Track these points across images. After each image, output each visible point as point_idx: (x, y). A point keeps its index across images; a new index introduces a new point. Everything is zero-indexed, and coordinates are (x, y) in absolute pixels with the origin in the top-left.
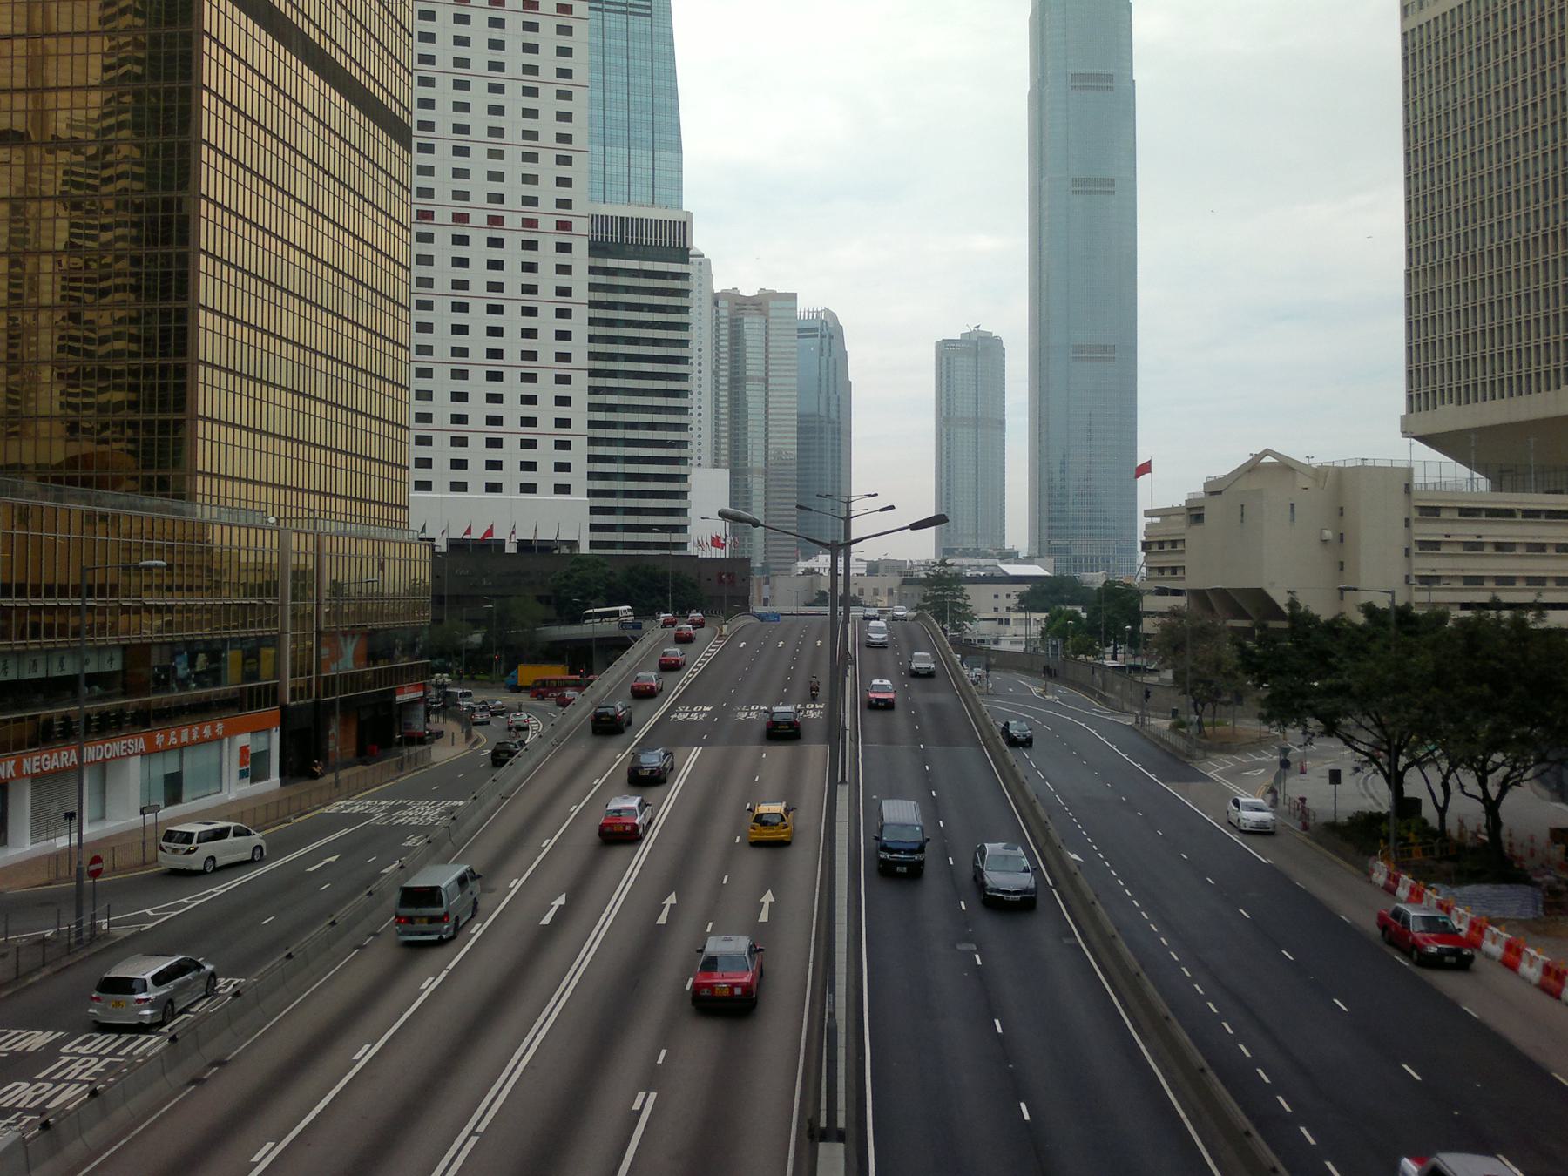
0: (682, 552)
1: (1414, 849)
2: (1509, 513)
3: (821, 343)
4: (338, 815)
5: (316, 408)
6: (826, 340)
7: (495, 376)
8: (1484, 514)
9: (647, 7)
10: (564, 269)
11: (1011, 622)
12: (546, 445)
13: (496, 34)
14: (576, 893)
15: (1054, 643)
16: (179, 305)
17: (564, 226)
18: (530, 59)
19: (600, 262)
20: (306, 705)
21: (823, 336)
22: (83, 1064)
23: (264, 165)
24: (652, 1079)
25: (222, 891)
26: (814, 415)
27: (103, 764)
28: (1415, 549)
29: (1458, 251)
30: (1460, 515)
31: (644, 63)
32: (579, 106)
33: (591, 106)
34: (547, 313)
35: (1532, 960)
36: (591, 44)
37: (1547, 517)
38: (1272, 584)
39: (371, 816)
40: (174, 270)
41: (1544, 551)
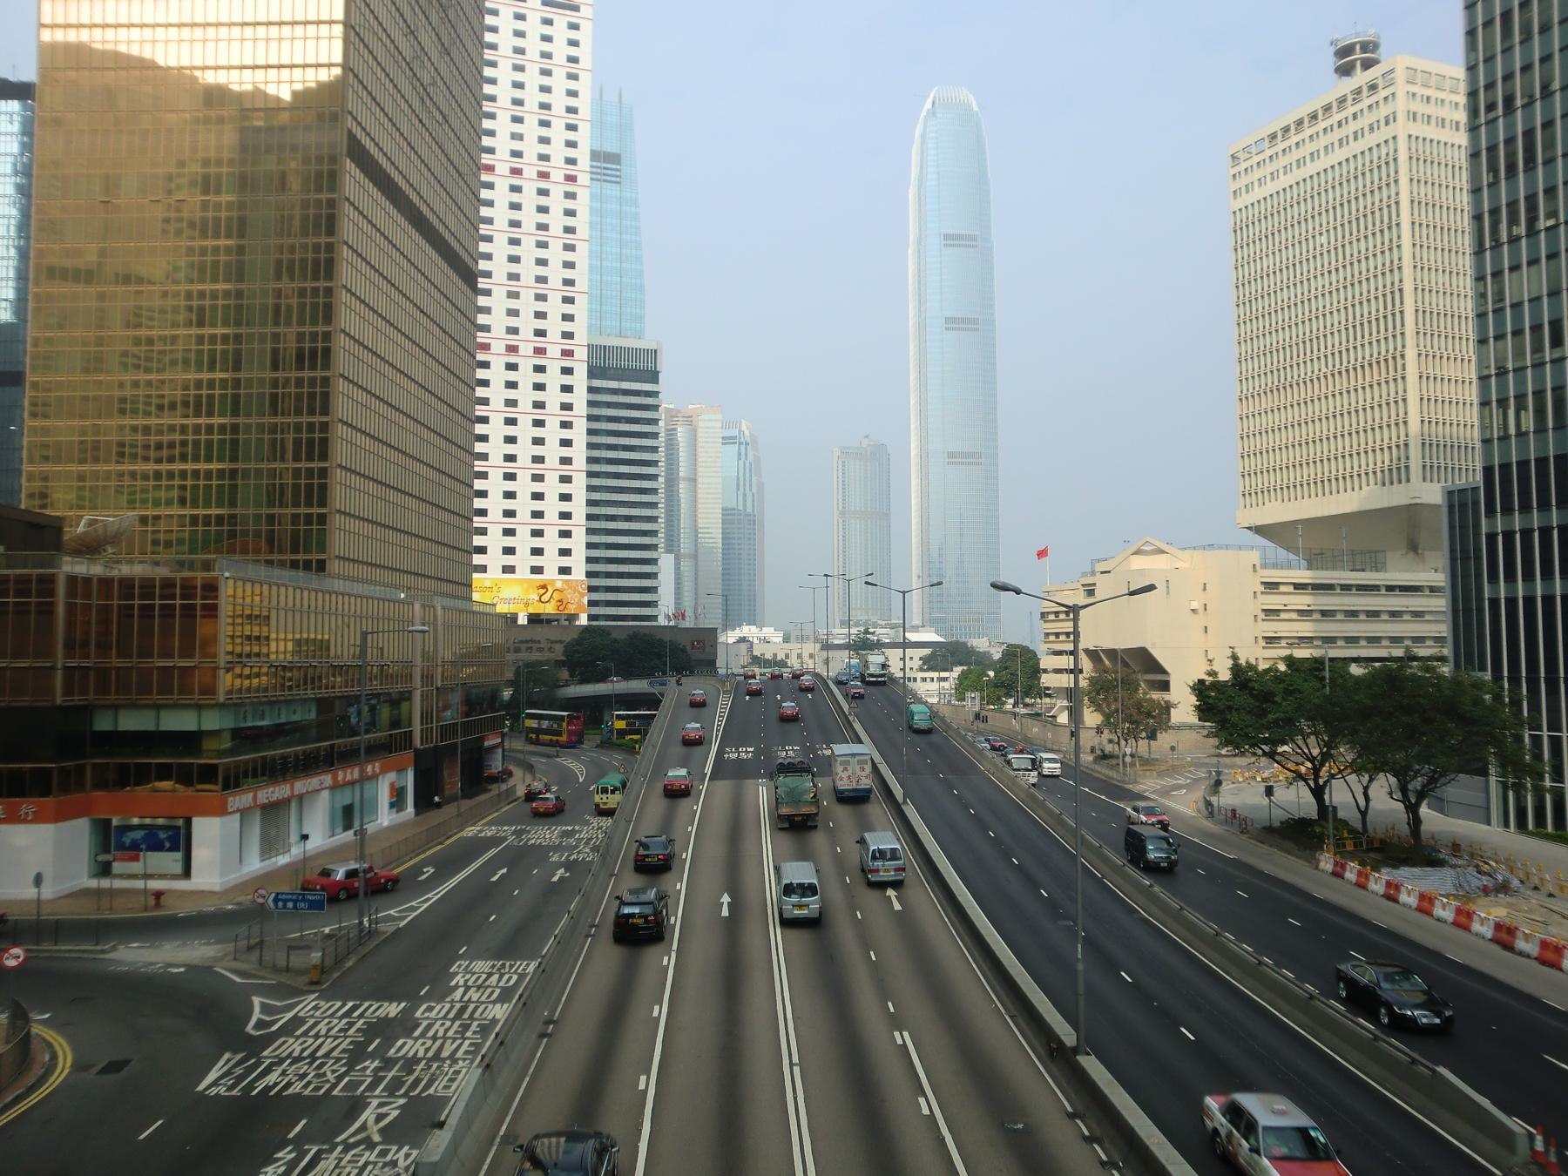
0: (654, 624)
1: (1347, 842)
2: (1330, 587)
3: (739, 449)
4: (475, 839)
5: (412, 503)
6: (743, 447)
7: (510, 477)
8: (1310, 587)
9: (617, 176)
10: (567, 389)
11: (918, 680)
12: (551, 533)
13: (516, 198)
14: (734, 887)
15: (973, 695)
16: (324, 419)
17: (568, 353)
18: (542, 218)
19: (597, 383)
20: (429, 748)
21: (740, 443)
22: (302, 1044)
23: (381, 304)
24: (896, 1022)
25: (437, 897)
26: (734, 509)
27: (301, 797)
28: (1262, 616)
29: (1279, 381)
30: (1295, 588)
31: (614, 221)
32: (581, 256)
33: (591, 257)
34: (553, 424)
35: (1483, 921)
36: (591, 208)
37: (1357, 590)
38: (1153, 644)
39: (505, 839)
40: (318, 390)
41: (1378, 616)
